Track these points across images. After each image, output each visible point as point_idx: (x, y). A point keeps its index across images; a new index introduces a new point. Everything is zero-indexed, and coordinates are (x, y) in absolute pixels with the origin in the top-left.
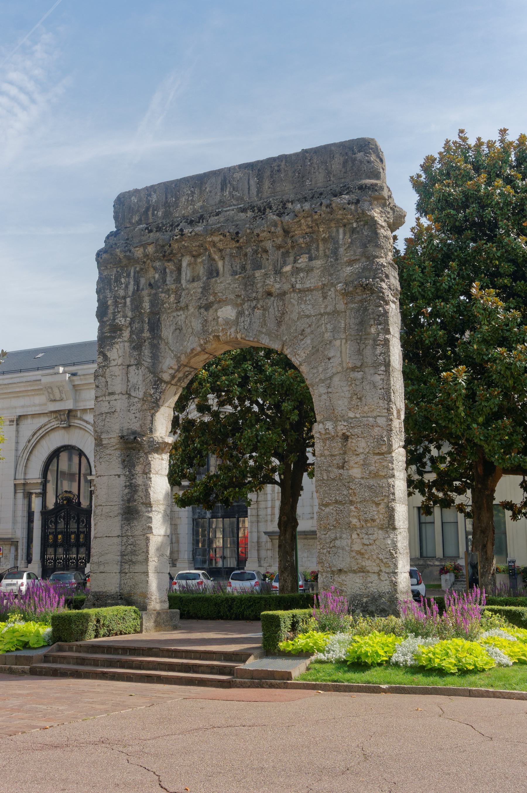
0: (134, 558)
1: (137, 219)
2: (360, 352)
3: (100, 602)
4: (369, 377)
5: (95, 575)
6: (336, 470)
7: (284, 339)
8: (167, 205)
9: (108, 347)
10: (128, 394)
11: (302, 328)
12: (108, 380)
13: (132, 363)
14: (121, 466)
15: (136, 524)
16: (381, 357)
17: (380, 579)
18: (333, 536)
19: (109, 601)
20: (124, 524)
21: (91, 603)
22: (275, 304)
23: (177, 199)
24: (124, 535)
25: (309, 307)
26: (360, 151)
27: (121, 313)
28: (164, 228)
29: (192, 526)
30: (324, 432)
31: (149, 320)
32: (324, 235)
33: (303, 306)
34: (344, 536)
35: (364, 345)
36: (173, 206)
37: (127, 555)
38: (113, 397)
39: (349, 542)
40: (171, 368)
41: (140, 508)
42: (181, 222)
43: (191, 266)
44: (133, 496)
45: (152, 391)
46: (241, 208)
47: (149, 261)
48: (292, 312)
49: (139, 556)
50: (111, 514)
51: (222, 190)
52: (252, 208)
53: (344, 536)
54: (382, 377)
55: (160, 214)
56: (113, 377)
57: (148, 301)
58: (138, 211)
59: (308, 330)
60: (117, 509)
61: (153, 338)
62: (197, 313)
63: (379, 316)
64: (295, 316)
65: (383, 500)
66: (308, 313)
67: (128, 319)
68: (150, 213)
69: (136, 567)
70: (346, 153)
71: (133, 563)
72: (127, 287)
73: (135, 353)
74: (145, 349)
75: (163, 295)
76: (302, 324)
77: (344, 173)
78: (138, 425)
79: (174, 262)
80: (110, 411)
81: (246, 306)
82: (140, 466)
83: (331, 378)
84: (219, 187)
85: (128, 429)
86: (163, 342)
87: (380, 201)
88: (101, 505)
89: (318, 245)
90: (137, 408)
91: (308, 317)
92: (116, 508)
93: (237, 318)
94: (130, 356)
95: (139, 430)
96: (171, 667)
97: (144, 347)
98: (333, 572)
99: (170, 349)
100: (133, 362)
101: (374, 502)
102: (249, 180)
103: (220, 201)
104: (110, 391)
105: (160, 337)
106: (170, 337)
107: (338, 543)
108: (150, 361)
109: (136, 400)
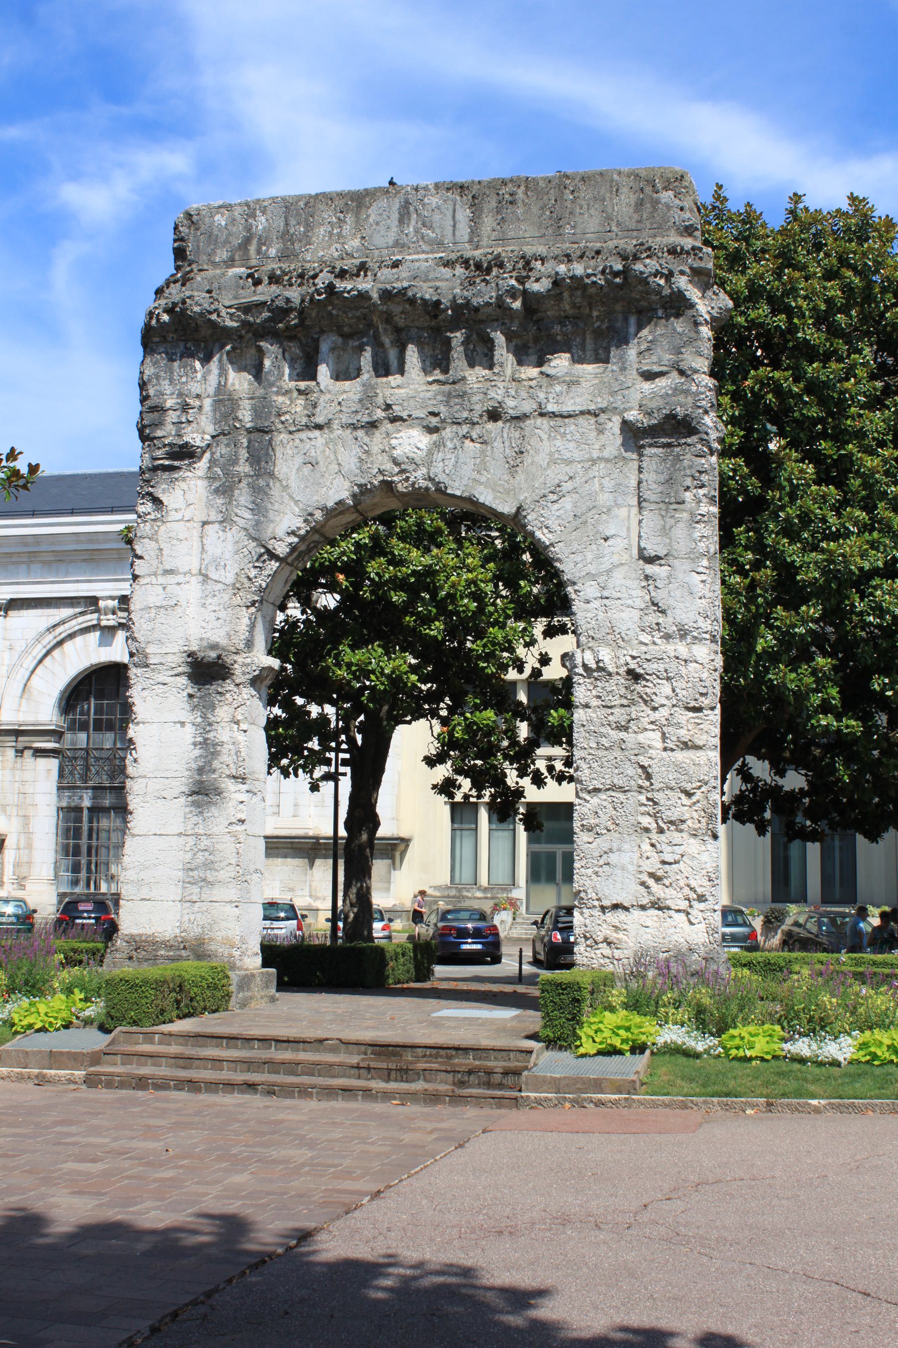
0: (210, 876)
1: (224, 257)
3: (144, 953)
4: (681, 576)
5: (130, 903)
7: (522, 498)
8: (286, 236)
9: (164, 486)
10: (203, 575)
11: (557, 481)
14: (187, 707)
15: (216, 814)
17: (691, 923)
18: (606, 846)
19: (162, 952)
20: (191, 812)
21: (125, 955)
22: (505, 435)
23: (309, 227)
24: (189, 833)
25: (572, 445)
26: (666, 189)
28: (286, 278)
29: (55, 819)
30: (594, 666)
31: (249, 442)
32: (598, 324)
33: (558, 443)
34: (626, 846)
35: (672, 521)
36: (300, 241)
37: (196, 869)
38: (171, 579)
40: (293, 533)
41: (223, 785)
42: (321, 271)
43: (336, 353)
44: (210, 763)
45: (253, 573)
46: (441, 258)
47: (250, 335)
48: (537, 452)
49: (222, 872)
50: (165, 794)
51: (401, 221)
52: (466, 263)
53: (626, 846)
55: (273, 252)
56: (175, 542)
57: (248, 407)
58: (227, 242)
59: (567, 486)
60: (181, 785)
61: (258, 475)
62: (351, 437)
63: (700, 472)
64: (542, 459)
65: (699, 788)
66: (567, 455)
68: (252, 248)
69: (214, 892)
70: (642, 189)
71: (211, 884)
73: (220, 501)
74: (240, 495)
75: (280, 399)
76: (555, 475)
77: (638, 222)
78: (222, 632)
79: (301, 343)
80: (165, 603)
82: (226, 708)
83: (609, 572)
84: (395, 216)
85: (201, 639)
86: (278, 484)
87: (702, 277)
88: (144, 777)
89: (584, 340)
90: (222, 601)
91: (569, 462)
94: (209, 505)
97: (237, 492)
98: (603, 909)
99: (291, 497)
100: (214, 516)
102: (454, 211)
103: (397, 244)
104: (168, 568)
105: (272, 475)
106: (293, 476)
107: (613, 858)
108: (251, 517)
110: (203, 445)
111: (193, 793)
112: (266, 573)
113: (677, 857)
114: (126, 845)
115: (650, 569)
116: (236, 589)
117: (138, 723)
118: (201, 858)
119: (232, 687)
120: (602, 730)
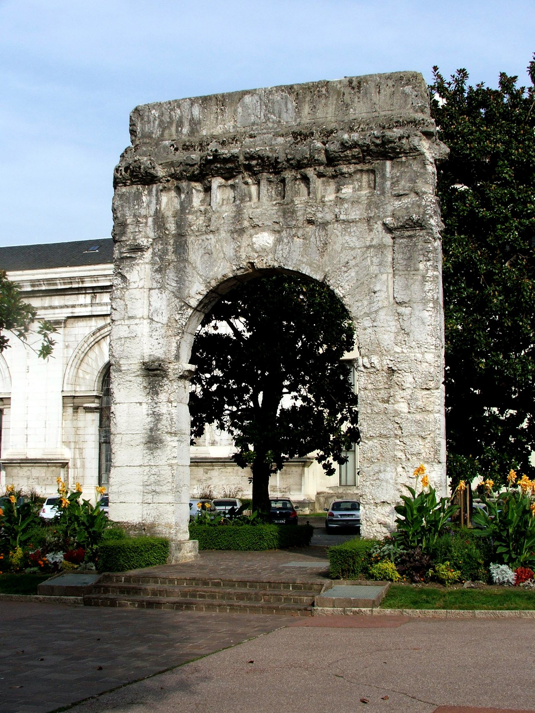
16: (429, 294)
25: (354, 239)
41: (164, 438)
44: (156, 425)
45: (178, 317)
49: (164, 487)
50: (132, 443)
59: (352, 263)
72: (148, 206)
73: (158, 276)
78: (161, 351)
81: (284, 234)
83: (376, 312)
91: (353, 249)
95: (163, 357)
109: (160, 325)
114: (112, 472)
115: (401, 310)
116: (168, 326)
117: (116, 404)
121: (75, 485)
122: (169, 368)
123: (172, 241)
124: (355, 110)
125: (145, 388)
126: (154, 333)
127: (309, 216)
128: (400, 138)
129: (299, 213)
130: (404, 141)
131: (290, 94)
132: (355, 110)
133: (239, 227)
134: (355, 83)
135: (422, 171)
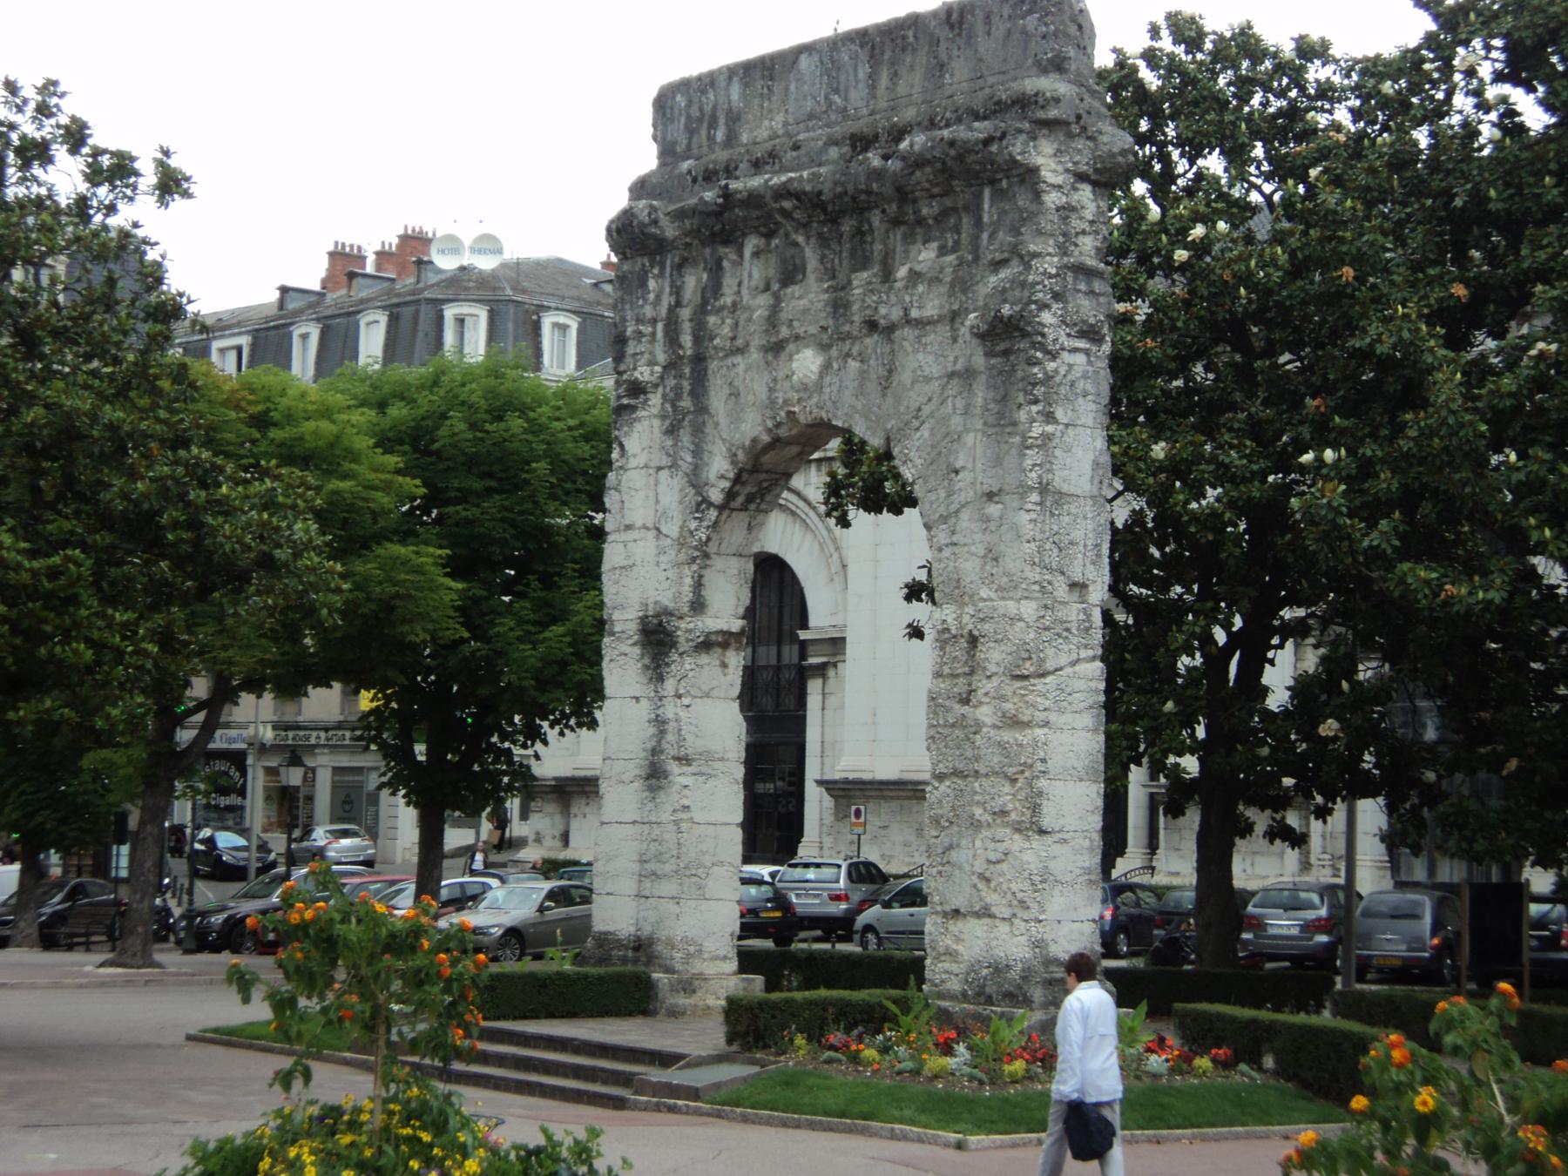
2: (998, 461)
6: (957, 706)
12: (625, 497)
13: (664, 463)
16: (1034, 475)
27: (646, 356)
39: (971, 853)
44: (659, 742)
45: (693, 525)
54: (1033, 516)
59: (926, 410)
65: (1022, 772)
67: (658, 369)
72: (658, 298)
78: (669, 594)
83: (957, 512)
92: (631, 765)
93: (821, 375)
95: (671, 605)
96: (501, 1060)
101: (1006, 777)
109: (669, 542)
110: (653, 379)
111: (648, 778)
112: (705, 524)
113: (1000, 856)
118: (654, 847)
119: (675, 657)
120: (947, 703)
121: (1327, 856)
122: (678, 628)
123: (687, 371)
124: (952, 75)
125: (646, 667)
126: (662, 558)
127: (868, 312)
128: (987, 141)
129: (855, 307)
130: (994, 148)
131: (862, 46)
132: (952, 75)
133: (773, 339)
134: (955, 16)
135: (1034, 207)
